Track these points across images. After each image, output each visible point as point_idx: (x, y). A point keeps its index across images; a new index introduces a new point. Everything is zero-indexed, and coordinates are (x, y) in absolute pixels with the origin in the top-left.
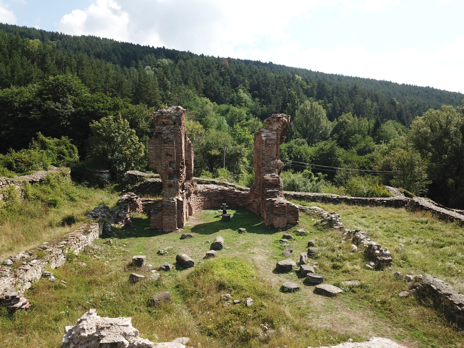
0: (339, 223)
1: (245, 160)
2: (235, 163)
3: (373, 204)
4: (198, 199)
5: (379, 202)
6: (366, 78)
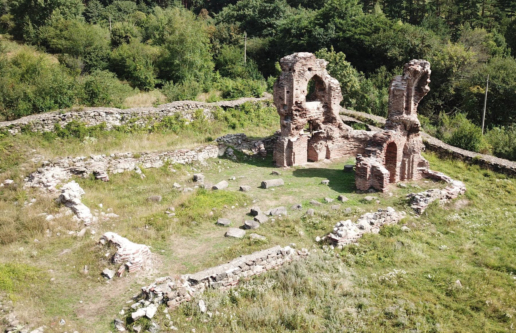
4: (350, 144)
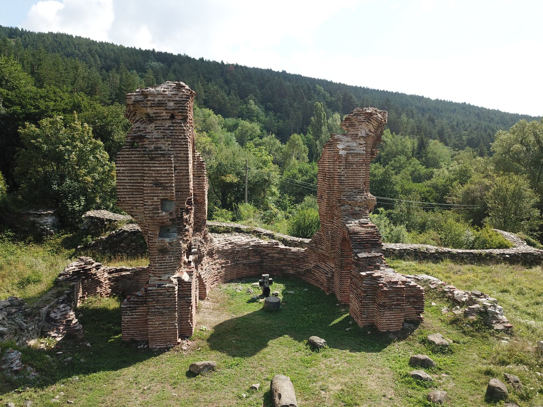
0: (500, 317)
1: (274, 189)
2: (260, 194)
3: (490, 260)
5: (499, 257)
6: (394, 92)
